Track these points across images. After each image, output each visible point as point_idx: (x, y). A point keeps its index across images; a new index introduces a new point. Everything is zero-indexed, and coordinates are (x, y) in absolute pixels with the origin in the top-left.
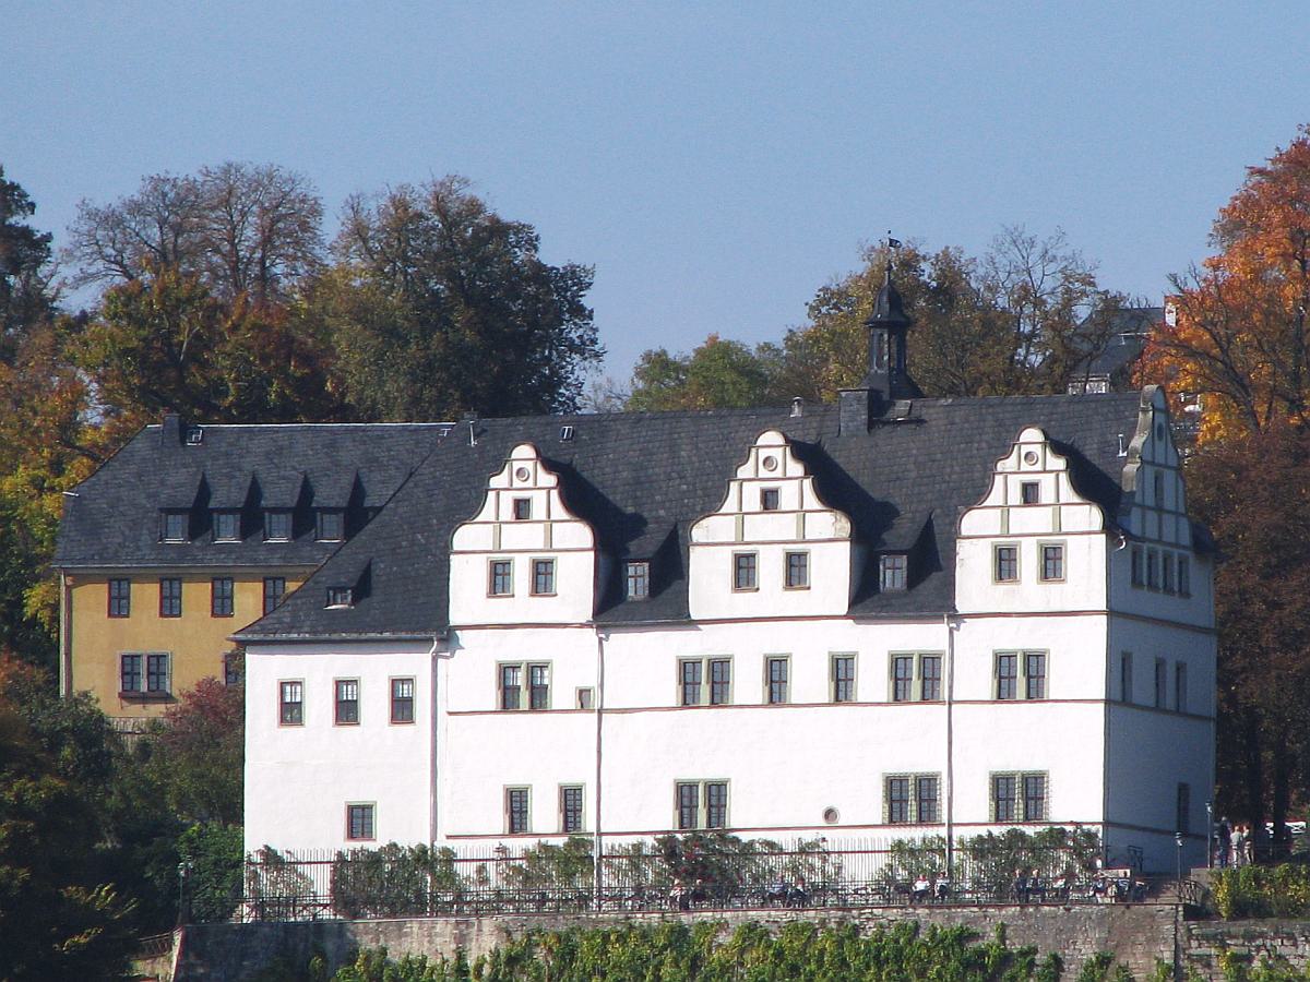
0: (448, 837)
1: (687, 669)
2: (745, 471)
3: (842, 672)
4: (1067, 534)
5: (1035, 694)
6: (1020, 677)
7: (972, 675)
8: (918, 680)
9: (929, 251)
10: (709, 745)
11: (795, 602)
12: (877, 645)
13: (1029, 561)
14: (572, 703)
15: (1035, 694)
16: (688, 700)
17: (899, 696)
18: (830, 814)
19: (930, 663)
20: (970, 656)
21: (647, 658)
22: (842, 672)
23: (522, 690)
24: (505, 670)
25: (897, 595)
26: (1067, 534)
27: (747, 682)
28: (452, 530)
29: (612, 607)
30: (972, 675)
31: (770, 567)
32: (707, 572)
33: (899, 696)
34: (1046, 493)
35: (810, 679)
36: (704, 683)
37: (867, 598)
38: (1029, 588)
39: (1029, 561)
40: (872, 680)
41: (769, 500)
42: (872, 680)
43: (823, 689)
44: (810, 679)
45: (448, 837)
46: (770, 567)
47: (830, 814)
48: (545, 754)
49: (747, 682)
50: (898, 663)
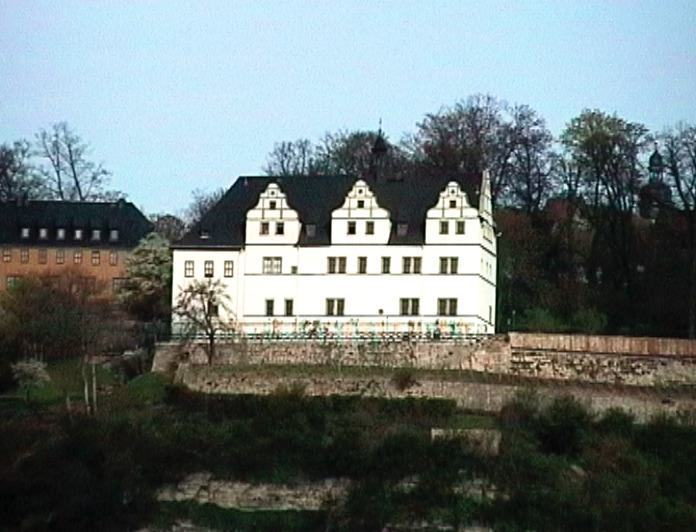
0: (245, 316)
1: (332, 260)
2: (351, 194)
3: (386, 261)
4: (467, 218)
5: (417, 271)
6: (449, 266)
7: (431, 264)
8: (412, 266)
9: (538, 110)
10: (336, 286)
11: (370, 239)
12: (398, 253)
13: (452, 227)
14: (289, 271)
15: (417, 271)
16: (443, 272)
17: (406, 272)
18: (381, 311)
19: (418, 260)
20: (430, 256)
21: (317, 256)
22: (386, 261)
23: (272, 264)
24: (444, 260)
25: (78, 241)
26: (467, 218)
27: (352, 266)
28: (332, 210)
29: (394, 240)
30: (431, 264)
31: (361, 227)
32: (338, 229)
33: (406, 272)
34: (367, 204)
35: (374, 265)
36: (336, 266)
37: (394, 240)
38: (272, 237)
39: (452, 227)
40: (396, 266)
41: (361, 204)
42: (396, 266)
43: (379, 269)
44: (374, 265)
45: (245, 316)
46: (361, 227)
47: (381, 311)
48: (279, 289)
49: (352, 266)
50: (407, 260)
